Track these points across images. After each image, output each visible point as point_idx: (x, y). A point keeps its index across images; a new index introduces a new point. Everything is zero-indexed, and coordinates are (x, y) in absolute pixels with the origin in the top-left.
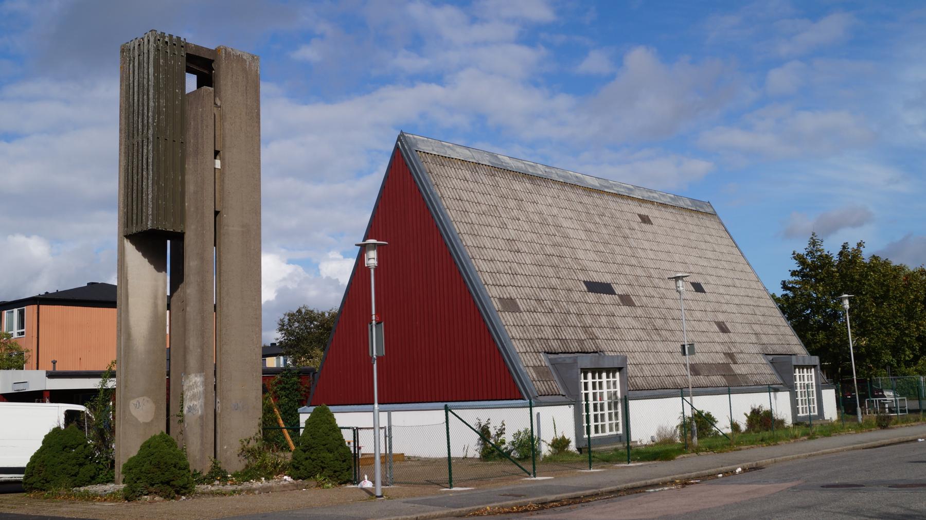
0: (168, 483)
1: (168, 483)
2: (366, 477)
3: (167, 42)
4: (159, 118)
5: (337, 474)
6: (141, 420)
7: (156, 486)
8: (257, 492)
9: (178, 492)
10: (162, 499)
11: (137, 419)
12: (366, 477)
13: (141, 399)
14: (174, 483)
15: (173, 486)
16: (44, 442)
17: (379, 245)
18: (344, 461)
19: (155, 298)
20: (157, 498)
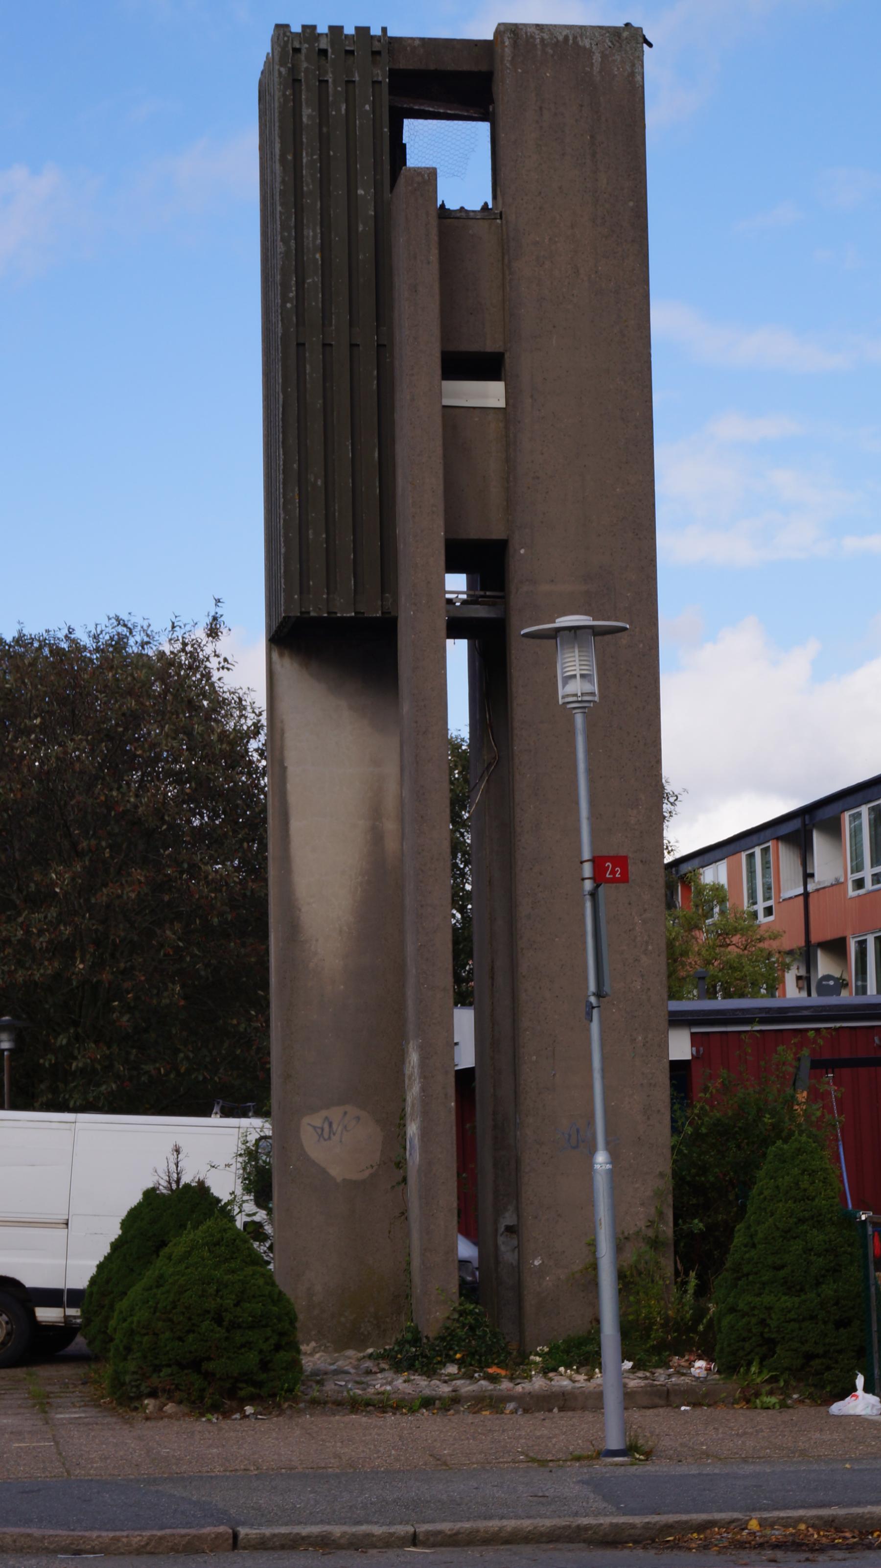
0: (196, 1365)
1: (196, 1365)
2: (860, 1381)
3: (323, 52)
4: (300, 284)
5: (816, 1363)
6: (336, 1172)
7: (165, 1371)
8: (511, 1406)
9: (231, 1393)
10: (184, 1408)
11: (324, 1172)
12: (860, 1381)
13: (335, 1113)
14: (210, 1366)
15: (209, 1376)
16: (124, 1224)
17: (596, 632)
18: (842, 1323)
19: (376, 813)
20: (170, 1408)
